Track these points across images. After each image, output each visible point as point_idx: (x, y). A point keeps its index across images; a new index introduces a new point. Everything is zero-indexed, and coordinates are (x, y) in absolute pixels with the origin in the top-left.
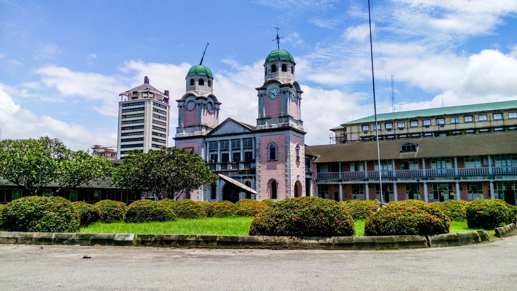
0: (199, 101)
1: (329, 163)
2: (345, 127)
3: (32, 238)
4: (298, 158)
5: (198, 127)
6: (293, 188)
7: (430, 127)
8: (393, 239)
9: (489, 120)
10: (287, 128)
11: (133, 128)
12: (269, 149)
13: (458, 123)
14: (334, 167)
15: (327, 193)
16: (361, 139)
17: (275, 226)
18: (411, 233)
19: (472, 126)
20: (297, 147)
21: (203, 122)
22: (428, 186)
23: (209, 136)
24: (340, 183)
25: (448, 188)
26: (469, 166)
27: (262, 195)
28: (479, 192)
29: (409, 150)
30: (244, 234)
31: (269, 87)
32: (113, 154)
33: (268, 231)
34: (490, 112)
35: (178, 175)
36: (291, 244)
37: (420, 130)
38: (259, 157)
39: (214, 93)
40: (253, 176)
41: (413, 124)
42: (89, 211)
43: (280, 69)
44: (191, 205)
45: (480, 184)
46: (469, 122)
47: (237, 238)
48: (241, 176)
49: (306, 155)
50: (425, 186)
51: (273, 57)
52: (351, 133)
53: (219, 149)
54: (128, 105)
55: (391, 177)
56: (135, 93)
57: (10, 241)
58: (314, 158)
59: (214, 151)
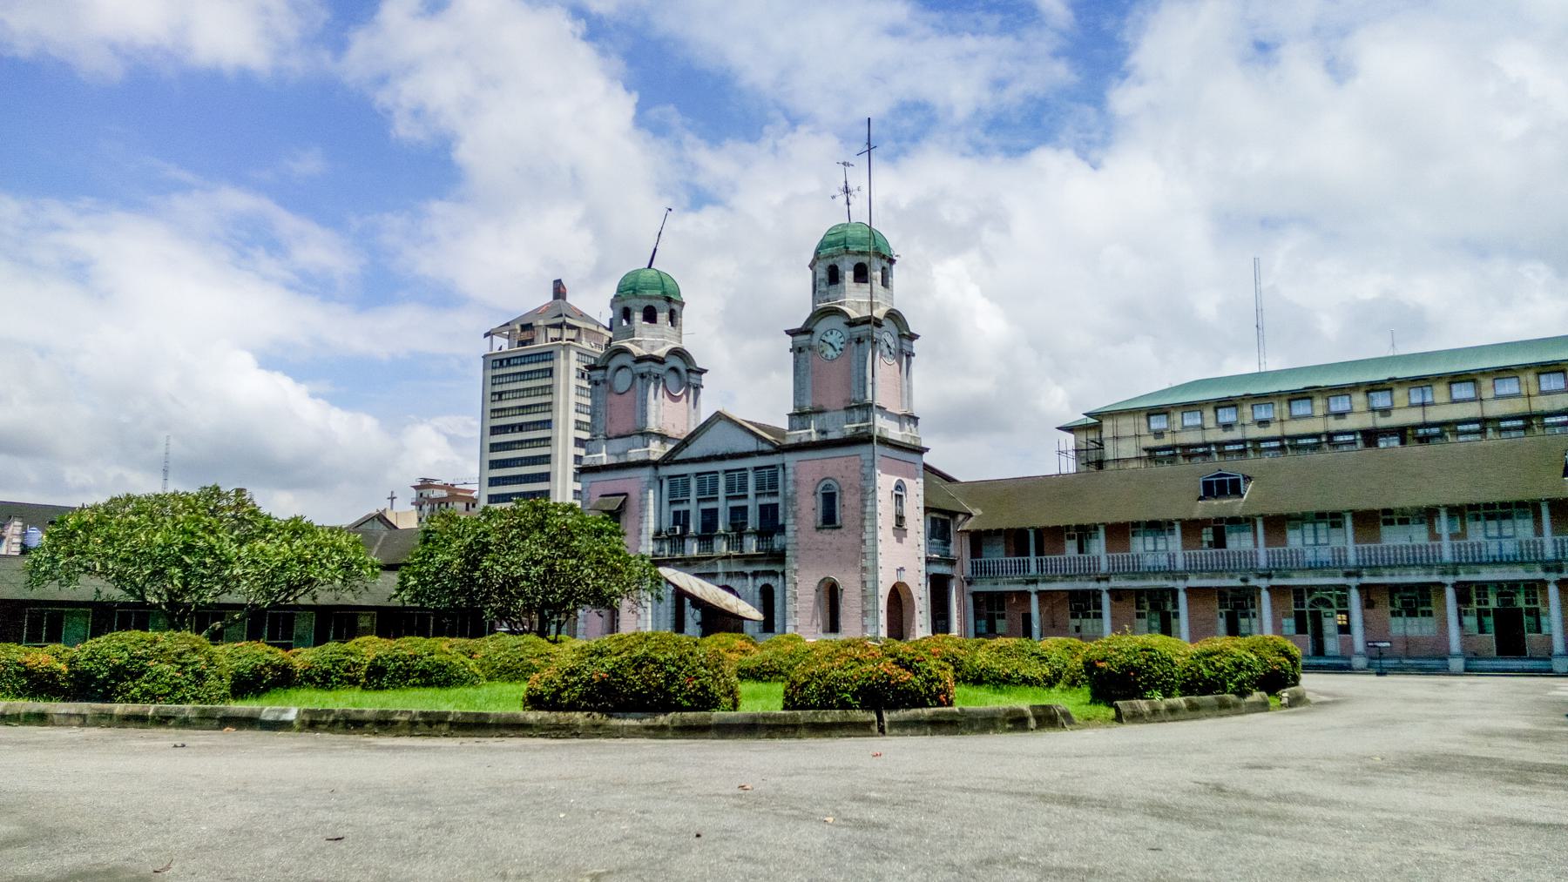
0: (644, 367)
1: (1009, 531)
2: (1098, 420)
3: (111, 715)
4: (900, 519)
5: (639, 438)
6: (883, 604)
7: (1349, 417)
8: (798, 718)
9: (1524, 392)
10: (863, 439)
11: (521, 430)
12: (820, 496)
13: (1433, 404)
14: (1017, 540)
15: (1003, 617)
16: (1145, 454)
17: (559, 691)
18: (844, 705)
19: (1472, 411)
20: (898, 487)
21: (652, 425)
22: (1272, 595)
23: (668, 460)
24: (1032, 588)
25: (1334, 601)
26: (1394, 538)
27: (802, 625)
28: (1423, 614)
29: (1222, 493)
30: (517, 710)
31: (821, 326)
32: (471, 503)
33: (547, 703)
34: (1527, 367)
35: (550, 570)
36: (586, 727)
37: (1317, 426)
38: (795, 517)
39: (687, 344)
40: (778, 569)
41: (1301, 408)
42: (269, 664)
43: (849, 275)
44: (531, 650)
45: (1424, 588)
47: (487, 715)
48: (749, 570)
49: (927, 510)
50: (1265, 595)
51: (831, 245)
52: (1116, 438)
53: (693, 496)
54: (509, 364)
55: (1170, 573)
56: (525, 327)
57: (73, 720)
58: (960, 518)
59: (682, 502)
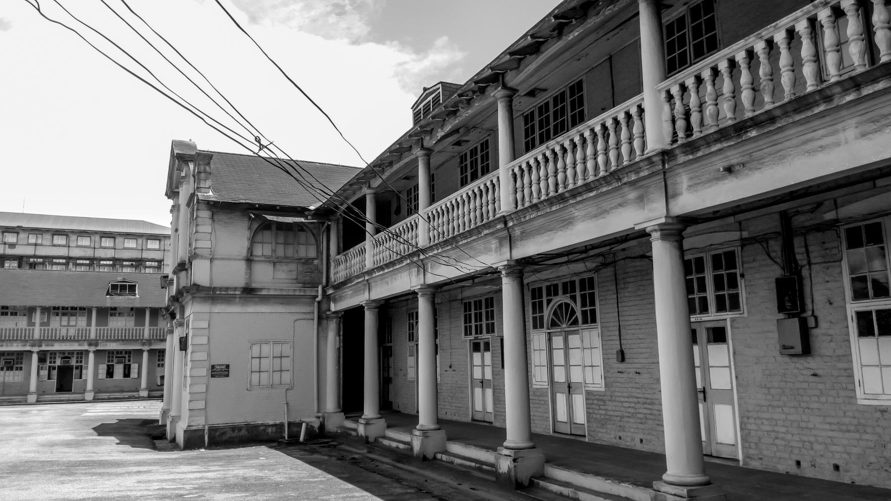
13: (41, 245)
19: (63, 252)
28: (17, 369)
34: (96, 233)
46: (59, 246)
